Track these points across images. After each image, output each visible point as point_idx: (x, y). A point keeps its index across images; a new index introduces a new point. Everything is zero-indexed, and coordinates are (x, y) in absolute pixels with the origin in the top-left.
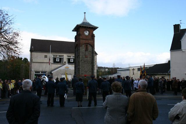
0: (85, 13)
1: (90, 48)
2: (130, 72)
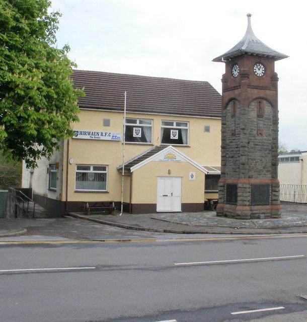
0: (249, 16)
1: (267, 109)
2: (115, 141)
